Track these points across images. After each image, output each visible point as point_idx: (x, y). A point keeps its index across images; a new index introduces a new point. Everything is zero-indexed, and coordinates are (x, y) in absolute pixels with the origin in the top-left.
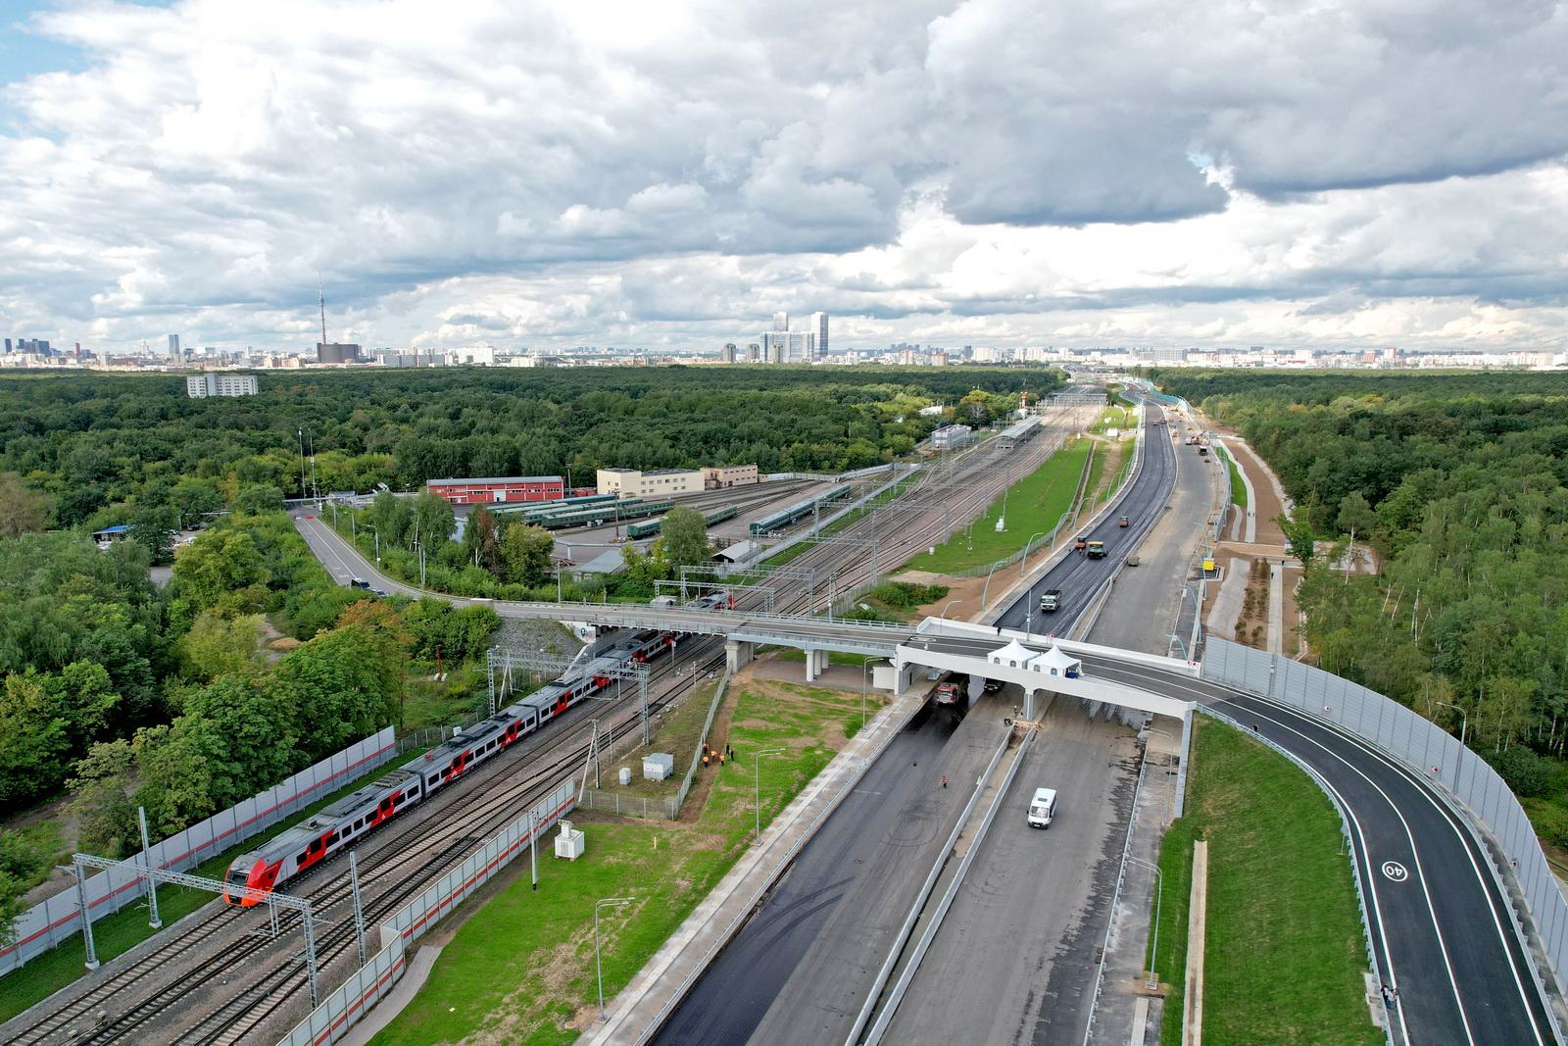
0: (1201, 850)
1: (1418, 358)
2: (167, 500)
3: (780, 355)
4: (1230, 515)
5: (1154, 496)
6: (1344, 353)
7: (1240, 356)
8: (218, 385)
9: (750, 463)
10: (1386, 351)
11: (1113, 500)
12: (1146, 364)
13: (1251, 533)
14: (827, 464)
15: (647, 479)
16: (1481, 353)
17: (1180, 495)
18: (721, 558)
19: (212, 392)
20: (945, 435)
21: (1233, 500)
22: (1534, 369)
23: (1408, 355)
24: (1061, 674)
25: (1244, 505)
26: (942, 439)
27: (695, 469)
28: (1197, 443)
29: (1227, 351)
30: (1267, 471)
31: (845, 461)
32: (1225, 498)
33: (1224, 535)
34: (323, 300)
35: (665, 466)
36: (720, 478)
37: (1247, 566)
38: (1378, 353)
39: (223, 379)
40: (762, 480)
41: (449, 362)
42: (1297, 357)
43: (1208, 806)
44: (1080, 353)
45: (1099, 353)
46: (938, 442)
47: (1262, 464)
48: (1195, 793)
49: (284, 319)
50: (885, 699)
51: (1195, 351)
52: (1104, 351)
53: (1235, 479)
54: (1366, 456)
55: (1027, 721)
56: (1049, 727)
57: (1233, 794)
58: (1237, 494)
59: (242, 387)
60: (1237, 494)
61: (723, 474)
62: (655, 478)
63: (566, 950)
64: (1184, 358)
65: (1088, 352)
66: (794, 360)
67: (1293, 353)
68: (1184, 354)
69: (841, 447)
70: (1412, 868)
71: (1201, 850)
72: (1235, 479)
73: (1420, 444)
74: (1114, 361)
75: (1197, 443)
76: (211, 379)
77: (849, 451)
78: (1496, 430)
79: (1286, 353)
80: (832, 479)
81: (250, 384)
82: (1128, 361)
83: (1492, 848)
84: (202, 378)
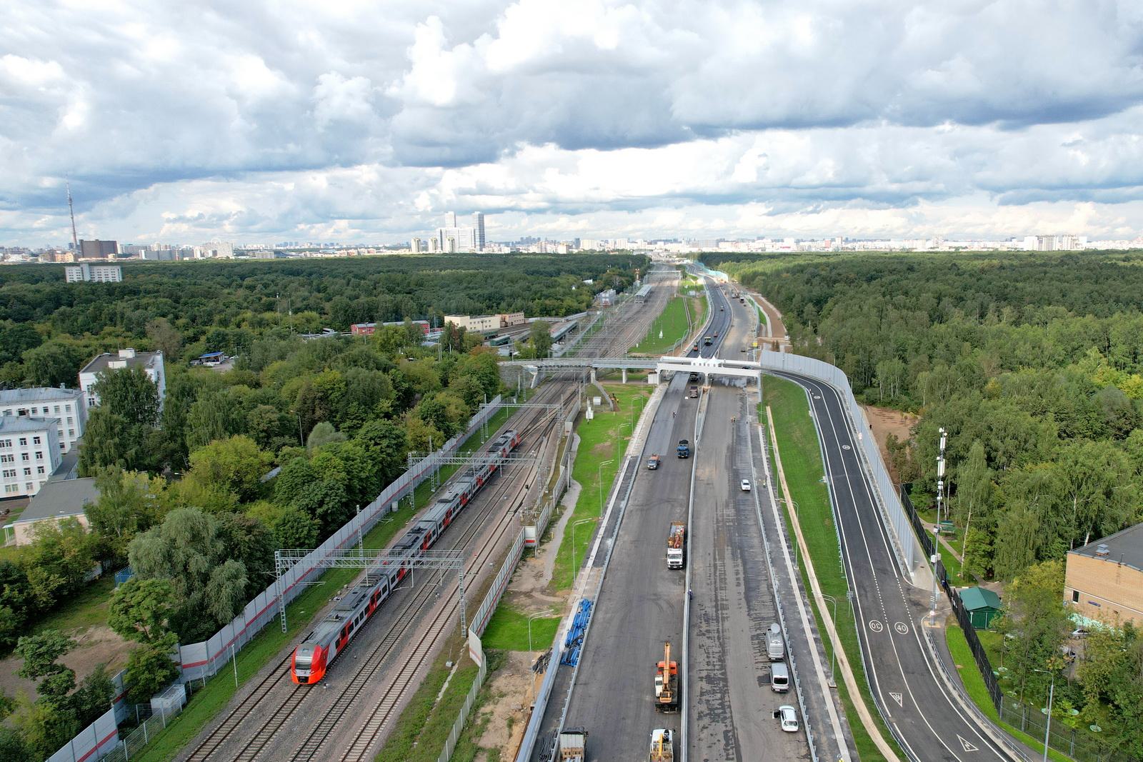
0: (768, 408)
1: (855, 244)
2: (227, 338)
3: (453, 246)
4: (760, 328)
5: (724, 322)
6: (813, 241)
7: (751, 244)
8: (91, 273)
9: (518, 311)
10: (837, 239)
11: (706, 323)
12: (695, 250)
13: (770, 334)
14: (554, 312)
15: (473, 320)
16: (889, 240)
17: (736, 321)
18: (91, 644)
19: (87, 278)
20: (607, 295)
21: (761, 322)
22: (915, 251)
23: (850, 242)
24: (717, 366)
25: (766, 324)
26: (606, 298)
27: (492, 315)
28: (738, 297)
29: (743, 241)
30: (774, 309)
31: (564, 310)
32: (757, 322)
33: (759, 335)
34: (71, 200)
35: (475, 314)
36: (507, 320)
37: (770, 346)
38: (833, 240)
39: (96, 268)
40: (527, 322)
41: (198, 256)
42: (785, 244)
43: (768, 398)
44: (650, 243)
45: (662, 243)
46: (604, 300)
47: (771, 306)
48: (764, 395)
49: (44, 219)
50: (651, 390)
51: (723, 240)
52: (666, 241)
53: (760, 314)
54: (817, 291)
55: (706, 386)
56: (713, 388)
57: (775, 393)
58: (762, 319)
59: (110, 276)
60: (762, 319)
61: (508, 318)
62: (477, 320)
63: (472, 635)
64: (717, 246)
65: (655, 242)
66: (439, 251)
67: (782, 241)
68: (719, 241)
69: (559, 302)
70: (841, 448)
71: (768, 408)
72: (760, 314)
73: (838, 286)
74: (674, 248)
75: (738, 297)
76: (86, 268)
77: (565, 304)
78: (870, 279)
79: (778, 241)
80: (563, 320)
81: (116, 273)
82: (685, 249)
83: (851, 419)
84: (78, 268)
